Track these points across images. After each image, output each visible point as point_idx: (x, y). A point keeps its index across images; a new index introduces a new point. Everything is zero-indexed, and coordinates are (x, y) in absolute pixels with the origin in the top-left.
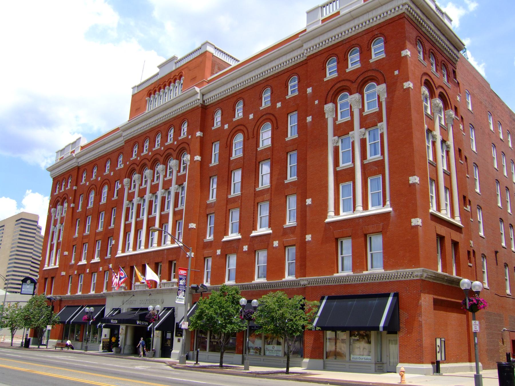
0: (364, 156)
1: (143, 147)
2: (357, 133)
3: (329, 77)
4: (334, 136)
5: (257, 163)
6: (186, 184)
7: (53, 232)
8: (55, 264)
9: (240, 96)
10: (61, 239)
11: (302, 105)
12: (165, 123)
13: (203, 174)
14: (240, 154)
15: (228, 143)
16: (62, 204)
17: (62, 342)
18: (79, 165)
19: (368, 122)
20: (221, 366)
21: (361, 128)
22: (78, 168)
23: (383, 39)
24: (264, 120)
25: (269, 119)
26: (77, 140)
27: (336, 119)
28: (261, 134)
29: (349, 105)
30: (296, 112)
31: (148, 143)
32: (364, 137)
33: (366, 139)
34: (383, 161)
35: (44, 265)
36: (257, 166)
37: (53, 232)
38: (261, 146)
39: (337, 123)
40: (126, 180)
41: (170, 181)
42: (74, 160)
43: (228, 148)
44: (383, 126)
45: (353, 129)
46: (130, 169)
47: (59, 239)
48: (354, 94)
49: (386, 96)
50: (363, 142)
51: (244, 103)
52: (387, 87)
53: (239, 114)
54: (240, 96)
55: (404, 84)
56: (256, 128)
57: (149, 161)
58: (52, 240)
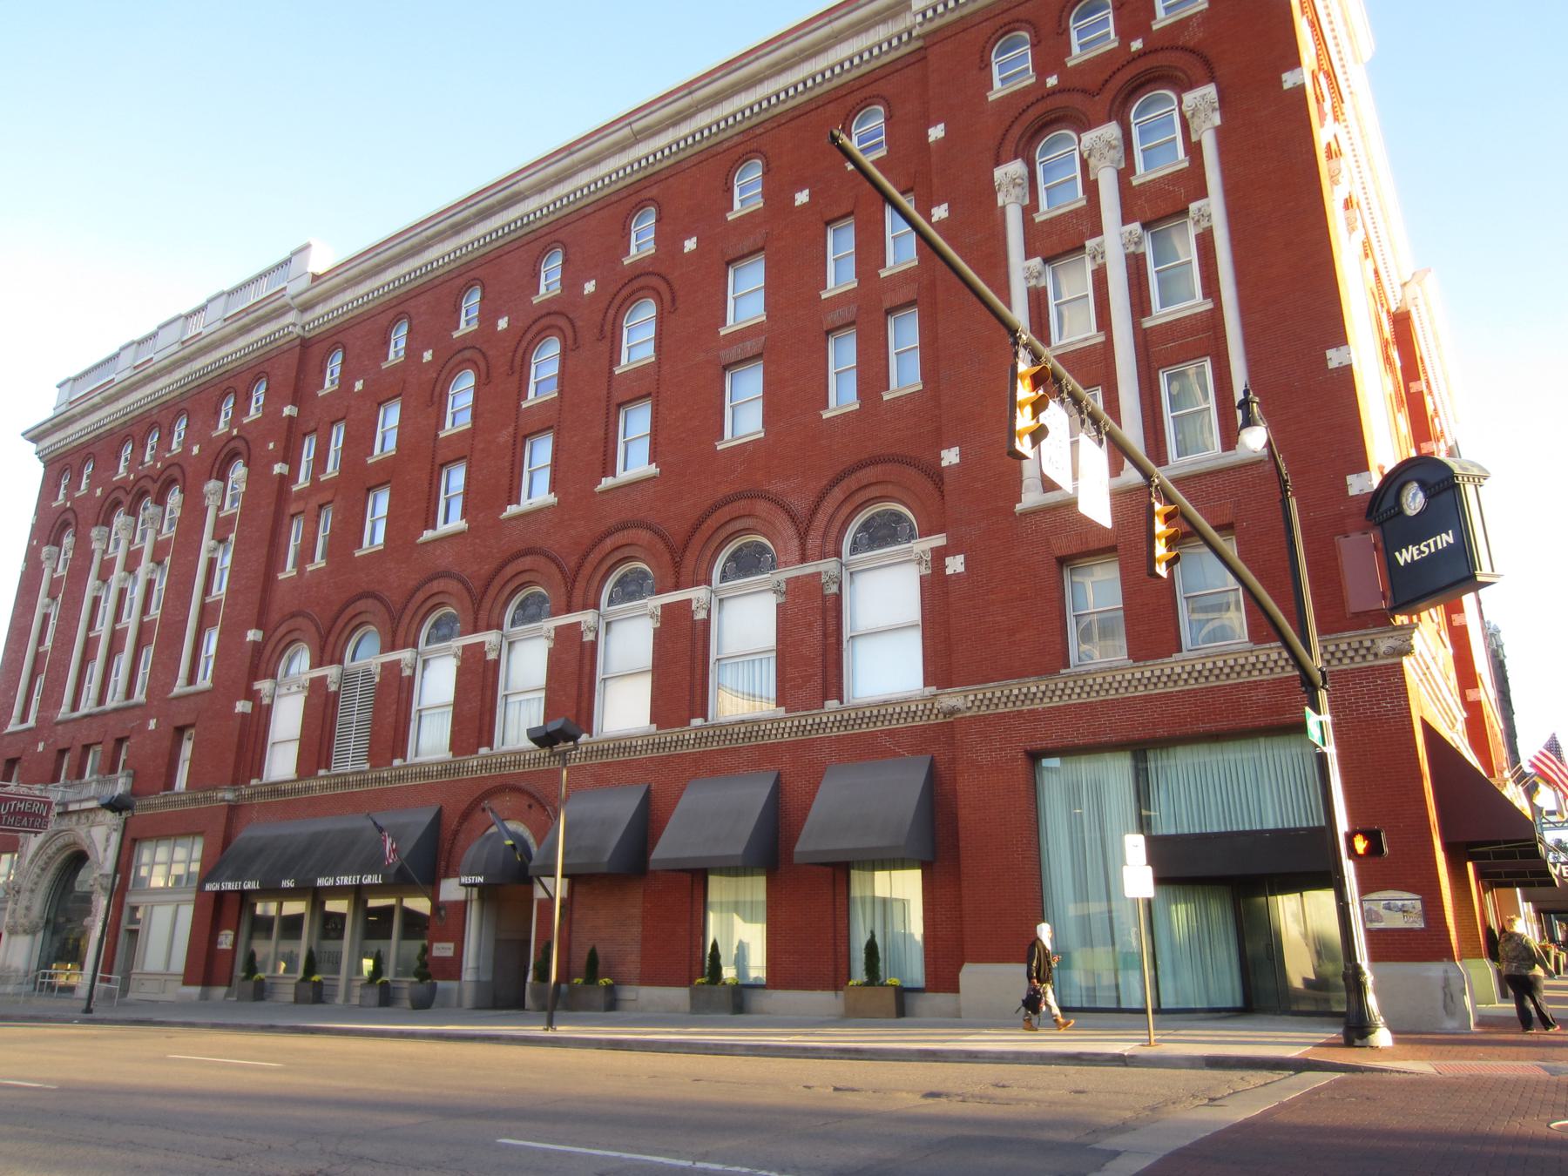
0: (1140, 305)
1: (249, 398)
2: (1115, 238)
3: (738, 209)
4: (1029, 255)
5: (520, 439)
6: (168, 560)
7: (96, 601)
8: (24, 719)
9: (400, 309)
10: (48, 643)
11: (919, 172)
12: (165, 406)
13: (272, 509)
14: (465, 421)
15: (608, 328)
16: (160, 501)
17: (426, 950)
18: (308, 335)
19: (1157, 207)
20: (1525, 1021)
21: (1027, 258)
22: (305, 344)
23: (1027, 35)
24: (461, 363)
25: (654, 289)
26: (294, 254)
27: (221, 508)
28: (533, 368)
29: (1078, 165)
30: (851, 220)
31: (262, 390)
32: (1141, 250)
33: (1045, 289)
34: (1216, 316)
35: (59, 704)
36: (612, 419)
37: (96, 601)
38: (624, 361)
39: (1039, 218)
40: (212, 485)
41: (140, 552)
42: (291, 317)
43: (516, 376)
44: (1213, 207)
45: (1097, 230)
46: (225, 451)
47: (41, 641)
48: (1006, 162)
49: (1217, 119)
50: (1136, 267)
51: (565, 255)
52: (1220, 92)
53: (467, 324)
54: (400, 309)
55: (1285, 76)
56: (611, 312)
57: (155, 481)
58: (91, 625)
